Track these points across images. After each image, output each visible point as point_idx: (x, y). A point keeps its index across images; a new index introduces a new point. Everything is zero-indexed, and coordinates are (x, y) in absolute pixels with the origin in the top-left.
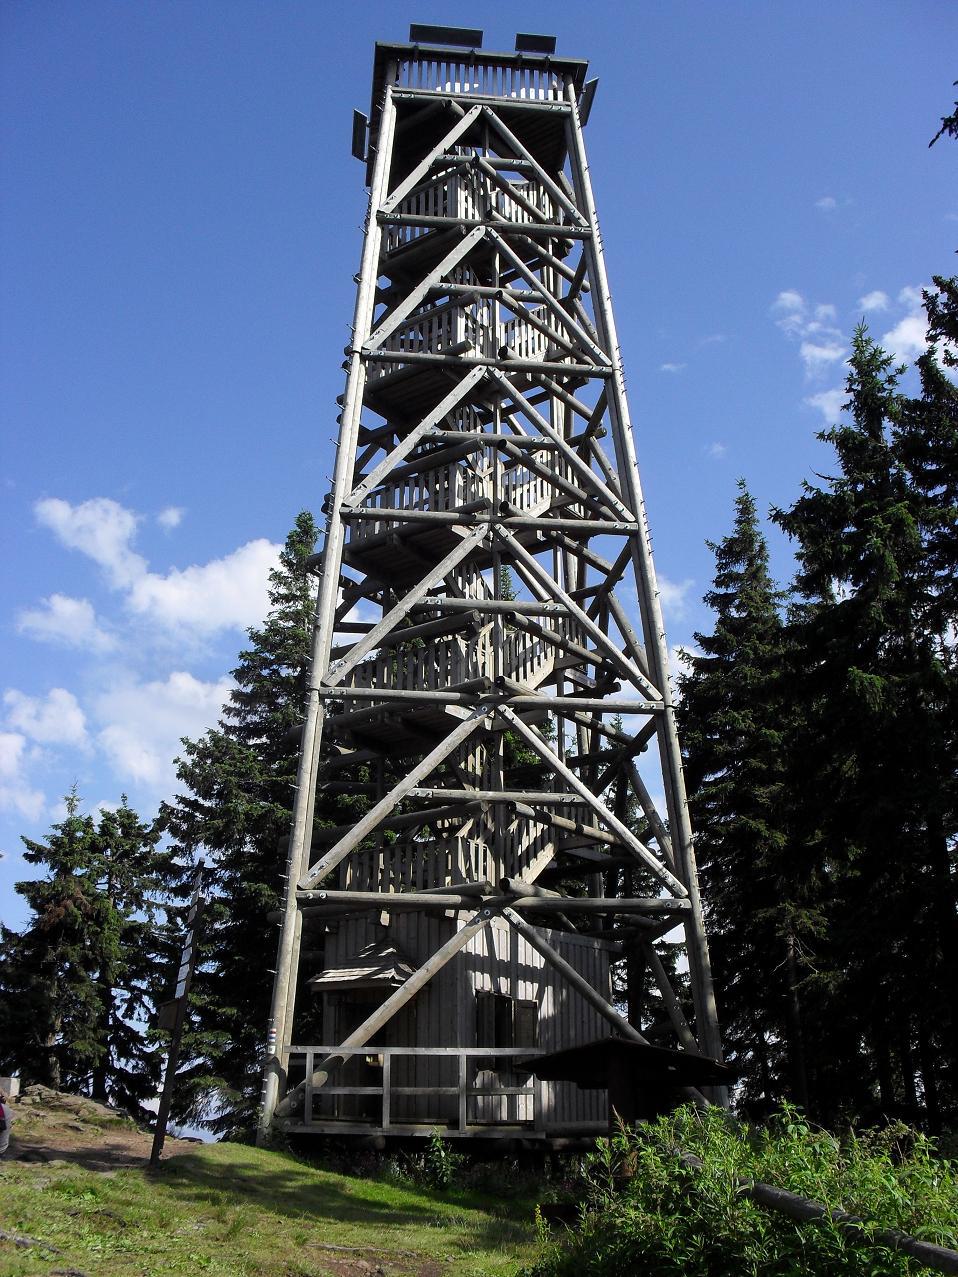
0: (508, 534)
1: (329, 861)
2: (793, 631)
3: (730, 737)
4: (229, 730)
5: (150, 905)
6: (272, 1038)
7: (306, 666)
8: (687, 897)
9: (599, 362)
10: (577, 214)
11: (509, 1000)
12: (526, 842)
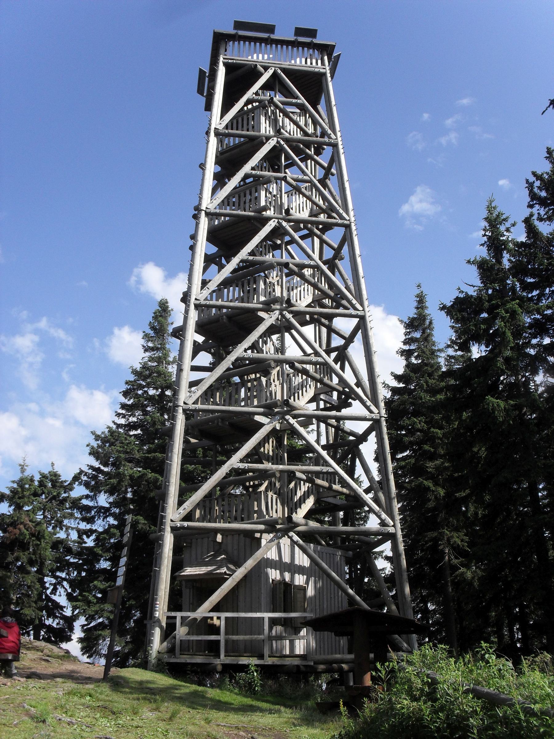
0: (289, 316)
1: (188, 505)
2: (450, 373)
3: (411, 432)
4: (119, 426)
5: (68, 528)
7: (176, 393)
8: (393, 526)
9: (342, 217)
10: (329, 132)
11: (290, 585)
12: (299, 494)
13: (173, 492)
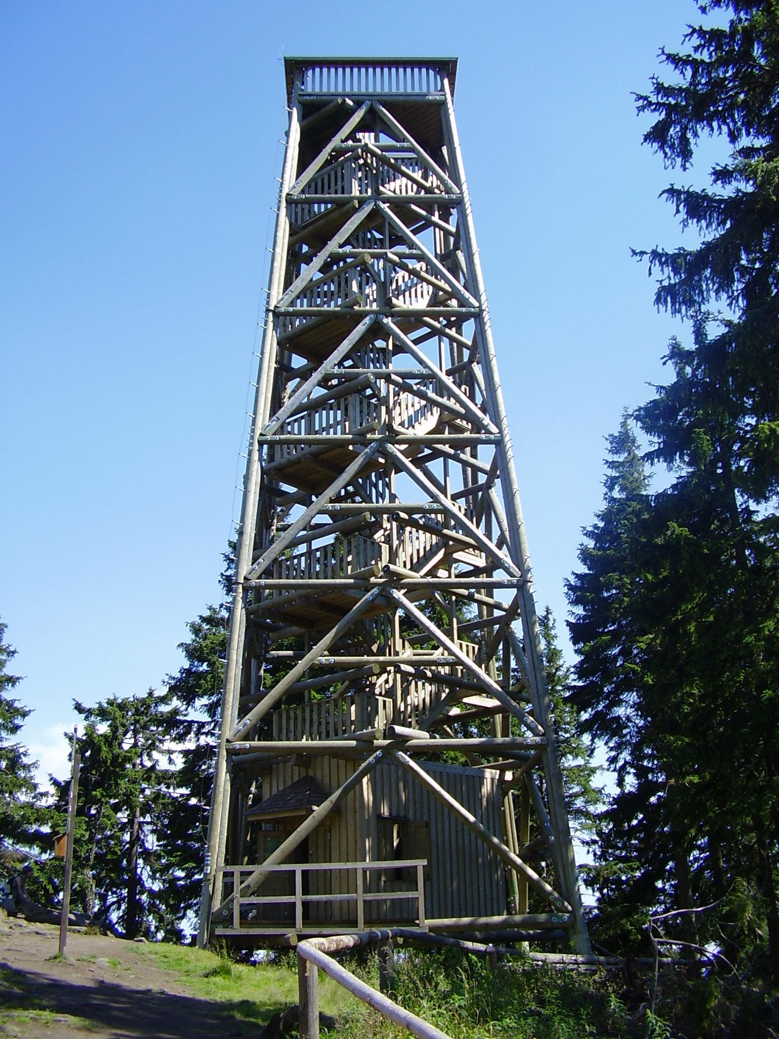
6: (208, 860)
13: (231, 701)
